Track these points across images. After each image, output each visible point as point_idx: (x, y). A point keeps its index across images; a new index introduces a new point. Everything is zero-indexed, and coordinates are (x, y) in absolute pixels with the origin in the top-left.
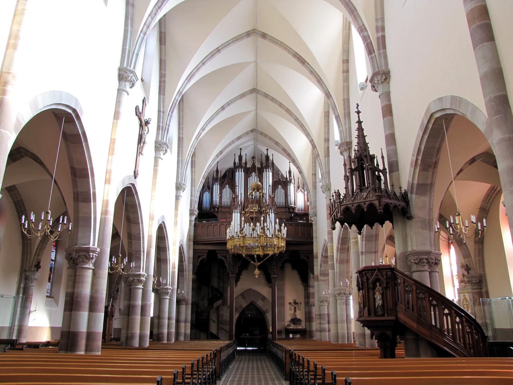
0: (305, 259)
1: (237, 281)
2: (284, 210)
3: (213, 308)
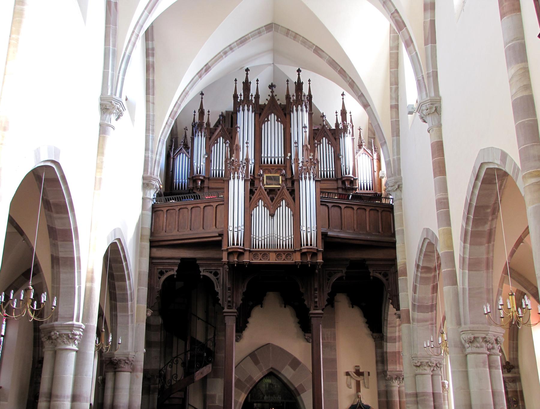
0: (380, 276)
1: (241, 327)
2: (333, 185)
3: (192, 381)
